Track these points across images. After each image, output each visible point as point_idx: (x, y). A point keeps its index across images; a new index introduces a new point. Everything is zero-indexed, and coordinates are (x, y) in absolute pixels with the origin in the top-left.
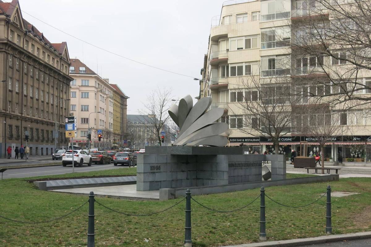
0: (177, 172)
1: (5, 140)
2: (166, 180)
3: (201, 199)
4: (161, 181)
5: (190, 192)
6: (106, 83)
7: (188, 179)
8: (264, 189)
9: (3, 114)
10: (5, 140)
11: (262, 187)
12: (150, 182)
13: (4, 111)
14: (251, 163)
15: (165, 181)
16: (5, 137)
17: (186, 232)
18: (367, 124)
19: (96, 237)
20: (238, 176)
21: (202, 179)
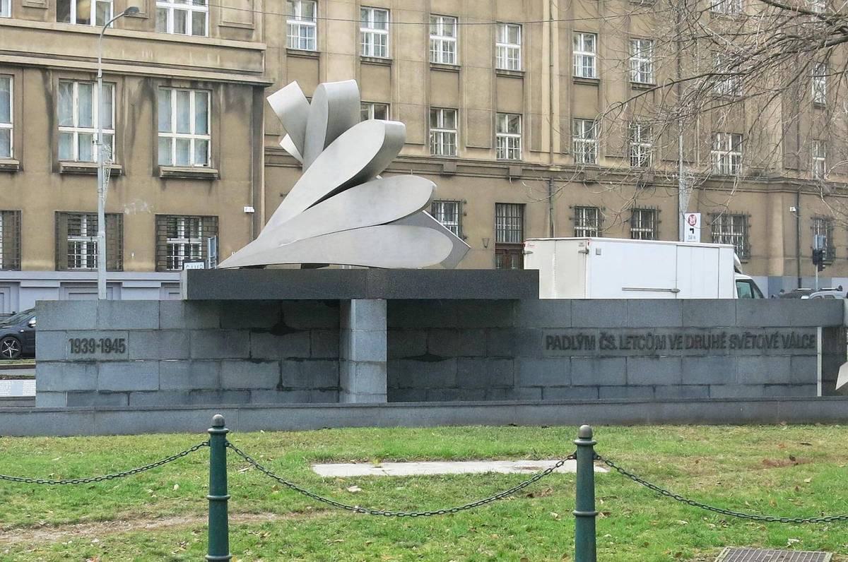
0: (219, 361)
1: (799, 270)
2: (156, 388)
3: (259, 449)
4: (128, 393)
5: (222, 427)
6: (29, 24)
7: (289, 389)
8: (590, 438)
9: (783, 182)
10: (799, 270)
11: (583, 427)
12: (70, 393)
13: (792, 175)
14: (724, 335)
15: (156, 391)
16: (798, 255)
17: (578, 526)
18: (245, 5)
19: (231, 505)
20: (626, 385)
21: (748, 385)
